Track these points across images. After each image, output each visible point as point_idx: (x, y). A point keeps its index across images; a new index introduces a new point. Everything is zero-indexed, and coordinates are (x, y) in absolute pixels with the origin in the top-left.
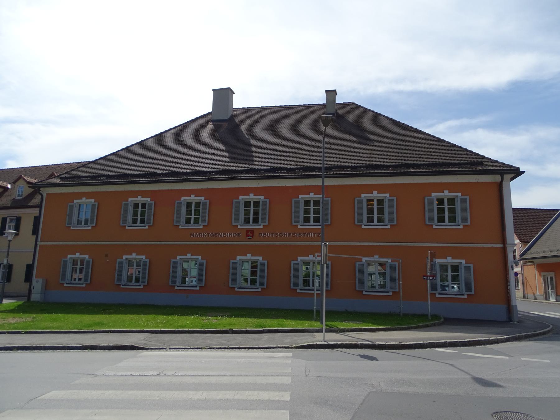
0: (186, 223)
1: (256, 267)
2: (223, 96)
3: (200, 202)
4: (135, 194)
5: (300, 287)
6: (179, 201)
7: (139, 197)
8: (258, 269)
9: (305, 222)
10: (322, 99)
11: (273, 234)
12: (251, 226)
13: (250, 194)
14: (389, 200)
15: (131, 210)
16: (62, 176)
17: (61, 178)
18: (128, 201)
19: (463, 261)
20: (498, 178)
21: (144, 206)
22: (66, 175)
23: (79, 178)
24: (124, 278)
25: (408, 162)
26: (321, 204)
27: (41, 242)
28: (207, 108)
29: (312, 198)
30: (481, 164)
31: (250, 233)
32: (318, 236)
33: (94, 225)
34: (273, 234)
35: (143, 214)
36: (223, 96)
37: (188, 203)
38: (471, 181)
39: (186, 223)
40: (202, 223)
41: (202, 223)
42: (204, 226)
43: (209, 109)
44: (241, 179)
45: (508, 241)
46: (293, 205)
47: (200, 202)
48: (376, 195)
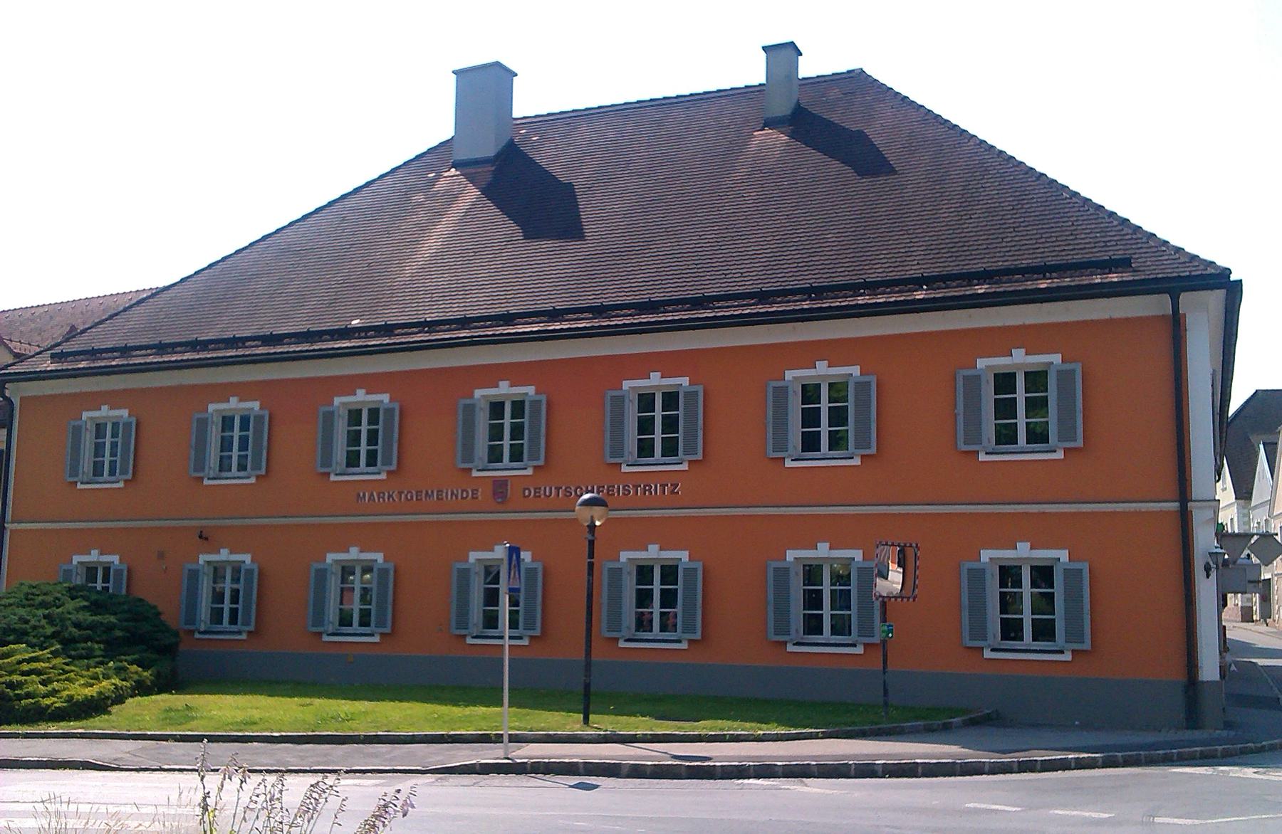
0: (348, 465)
1: (239, 571)
2: (484, 86)
3: (523, 402)
4: (642, 365)
5: (793, 635)
6: (615, 393)
7: (234, 400)
8: (853, 588)
9: (806, 448)
10: (754, 73)
11: (558, 489)
12: (506, 470)
13: (501, 383)
14: (1060, 373)
15: (483, 422)
16: (57, 350)
17: (53, 356)
18: (472, 396)
19: (1064, 555)
20: (1155, 305)
21: (518, 407)
22: (66, 347)
23: (93, 353)
24: (332, 613)
25: (914, 272)
26: (527, 412)
27: (12, 522)
28: (437, 124)
29: (1019, 366)
30: (1124, 264)
31: (500, 487)
32: (672, 492)
33: (129, 476)
34: (558, 489)
35: (517, 432)
36: (484, 86)
37: (224, 418)
38: (1027, 322)
39: (348, 465)
40: (383, 464)
41: (383, 464)
42: (535, 467)
43: (446, 131)
44: (472, 342)
45: (1197, 491)
46: (608, 408)
47: (523, 402)
48: (822, 370)
